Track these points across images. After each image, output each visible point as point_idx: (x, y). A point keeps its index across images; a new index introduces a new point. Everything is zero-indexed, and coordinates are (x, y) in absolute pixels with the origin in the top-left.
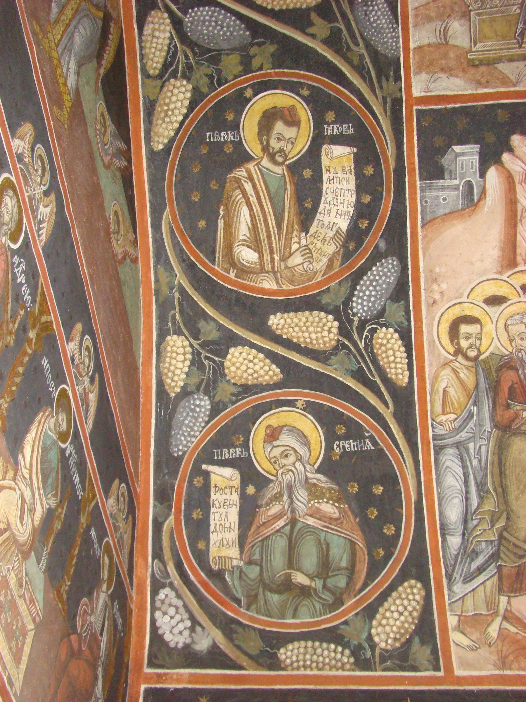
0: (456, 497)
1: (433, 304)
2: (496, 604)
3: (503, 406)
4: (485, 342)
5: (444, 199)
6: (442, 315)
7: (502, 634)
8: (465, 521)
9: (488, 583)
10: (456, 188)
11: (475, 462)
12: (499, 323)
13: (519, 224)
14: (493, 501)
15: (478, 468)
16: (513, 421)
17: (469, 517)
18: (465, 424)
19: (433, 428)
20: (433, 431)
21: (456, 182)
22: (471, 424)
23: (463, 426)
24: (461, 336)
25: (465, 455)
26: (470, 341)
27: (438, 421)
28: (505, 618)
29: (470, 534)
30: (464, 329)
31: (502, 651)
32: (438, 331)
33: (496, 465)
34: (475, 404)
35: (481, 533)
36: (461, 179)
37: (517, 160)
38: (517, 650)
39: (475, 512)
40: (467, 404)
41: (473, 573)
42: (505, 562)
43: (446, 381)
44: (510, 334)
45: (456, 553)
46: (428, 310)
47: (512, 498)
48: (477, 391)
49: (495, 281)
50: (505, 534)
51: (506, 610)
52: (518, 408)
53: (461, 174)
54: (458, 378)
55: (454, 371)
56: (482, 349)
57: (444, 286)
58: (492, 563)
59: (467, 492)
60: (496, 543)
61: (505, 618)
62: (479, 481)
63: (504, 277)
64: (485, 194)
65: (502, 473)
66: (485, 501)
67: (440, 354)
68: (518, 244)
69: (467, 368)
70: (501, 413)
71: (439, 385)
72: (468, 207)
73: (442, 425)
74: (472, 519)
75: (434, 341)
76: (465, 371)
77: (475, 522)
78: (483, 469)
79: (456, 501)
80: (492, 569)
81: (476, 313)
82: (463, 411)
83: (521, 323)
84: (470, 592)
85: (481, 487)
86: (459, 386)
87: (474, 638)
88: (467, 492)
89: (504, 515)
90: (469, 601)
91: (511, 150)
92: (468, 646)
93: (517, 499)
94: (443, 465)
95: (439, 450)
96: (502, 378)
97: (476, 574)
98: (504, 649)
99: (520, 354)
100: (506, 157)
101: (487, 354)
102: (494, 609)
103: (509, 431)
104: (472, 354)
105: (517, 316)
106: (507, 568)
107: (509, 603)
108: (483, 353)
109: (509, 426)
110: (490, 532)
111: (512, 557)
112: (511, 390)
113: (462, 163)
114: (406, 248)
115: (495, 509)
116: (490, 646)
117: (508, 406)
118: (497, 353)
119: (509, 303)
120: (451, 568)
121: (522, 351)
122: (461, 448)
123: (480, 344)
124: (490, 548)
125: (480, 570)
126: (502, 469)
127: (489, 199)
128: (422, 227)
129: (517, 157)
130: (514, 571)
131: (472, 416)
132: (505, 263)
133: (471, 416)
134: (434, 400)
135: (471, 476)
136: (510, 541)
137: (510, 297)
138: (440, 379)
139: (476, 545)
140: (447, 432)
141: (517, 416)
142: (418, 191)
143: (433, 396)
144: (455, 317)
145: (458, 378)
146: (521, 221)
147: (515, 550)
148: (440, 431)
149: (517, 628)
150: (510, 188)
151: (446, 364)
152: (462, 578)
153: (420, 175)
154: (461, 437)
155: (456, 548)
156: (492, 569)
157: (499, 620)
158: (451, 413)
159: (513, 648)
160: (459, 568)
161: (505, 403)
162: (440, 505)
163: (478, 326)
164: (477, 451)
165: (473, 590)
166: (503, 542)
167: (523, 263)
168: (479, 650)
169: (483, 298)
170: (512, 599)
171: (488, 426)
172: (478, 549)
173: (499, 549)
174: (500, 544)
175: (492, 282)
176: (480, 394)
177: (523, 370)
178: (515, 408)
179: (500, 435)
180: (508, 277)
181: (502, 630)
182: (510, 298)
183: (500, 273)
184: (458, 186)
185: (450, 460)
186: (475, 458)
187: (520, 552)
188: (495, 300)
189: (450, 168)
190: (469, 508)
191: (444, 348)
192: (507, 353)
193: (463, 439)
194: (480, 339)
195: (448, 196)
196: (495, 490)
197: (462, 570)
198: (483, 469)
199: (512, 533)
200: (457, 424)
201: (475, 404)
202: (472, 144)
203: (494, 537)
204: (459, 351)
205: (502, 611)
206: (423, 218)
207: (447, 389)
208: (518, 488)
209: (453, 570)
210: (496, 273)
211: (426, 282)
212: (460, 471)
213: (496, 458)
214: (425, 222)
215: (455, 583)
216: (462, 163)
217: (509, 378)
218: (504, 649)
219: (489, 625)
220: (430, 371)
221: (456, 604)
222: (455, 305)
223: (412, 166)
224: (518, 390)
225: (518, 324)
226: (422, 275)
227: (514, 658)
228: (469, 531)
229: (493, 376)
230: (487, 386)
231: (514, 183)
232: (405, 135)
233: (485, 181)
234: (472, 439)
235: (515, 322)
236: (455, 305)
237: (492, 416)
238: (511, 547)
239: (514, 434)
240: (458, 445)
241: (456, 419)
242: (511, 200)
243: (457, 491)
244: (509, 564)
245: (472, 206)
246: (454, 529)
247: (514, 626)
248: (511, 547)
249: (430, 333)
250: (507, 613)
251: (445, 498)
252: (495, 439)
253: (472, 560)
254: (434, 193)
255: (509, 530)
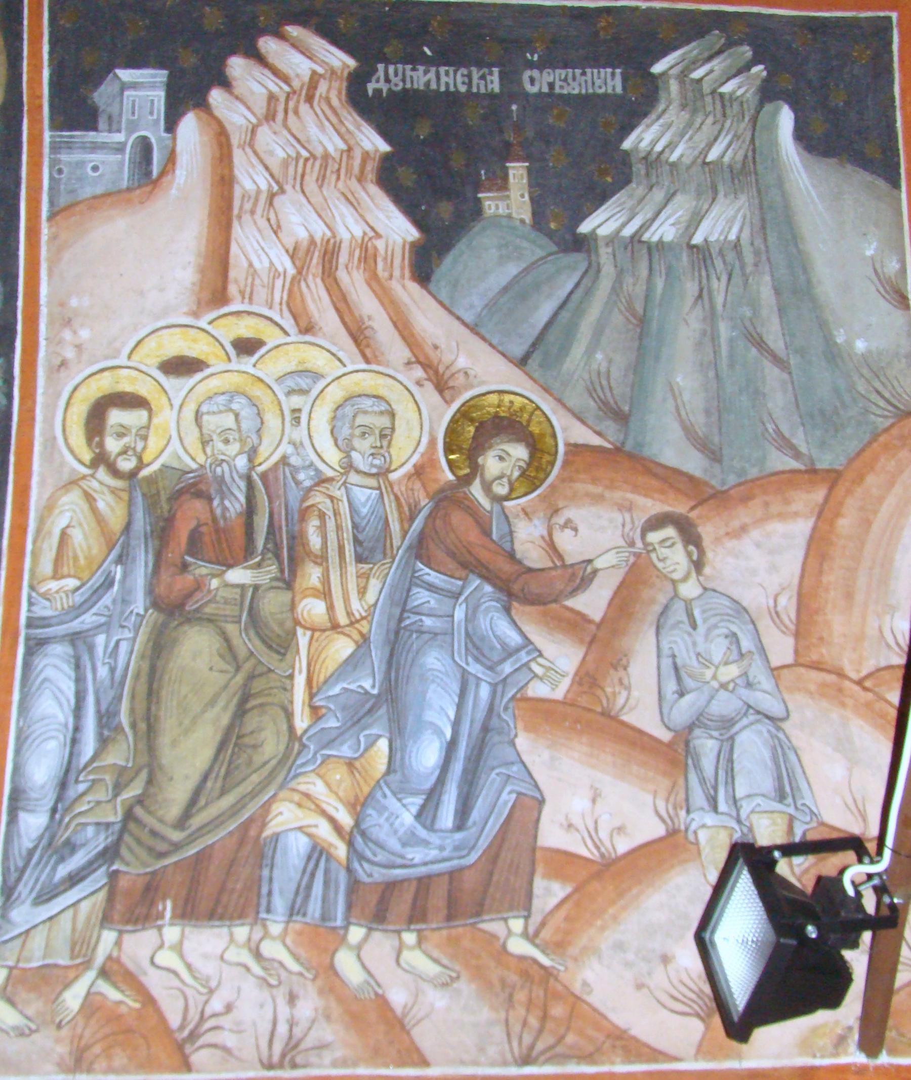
0: (52, 738)
1: (60, 366)
2: (92, 945)
3: (176, 565)
4: (154, 443)
5: (95, 169)
6: (75, 389)
7: (92, 1005)
8: (63, 785)
9: (85, 906)
10: (120, 148)
11: (103, 672)
12: (185, 409)
13: (235, 224)
14: (125, 746)
15: (107, 683)
16: (189, 595)
17: (72, 776)
18: (94, 598)
19: (31, 603)
20: (29, 611)
21: (119, 137)
22: (107, 600)
23: (90, 603)
24: (108, 430)
25: (86, 658)
26: (126, 440)
27: (43, 590)
28: (104, 973)
29: (67, 810)
30: (116, 417)
31: (81, 1037)
32: (64, 420)
33: (144, 679)
34: (120, 560)
35: (92, 809)
36: (130, 132)
37: (238, 104)
38: (113, 1034)
39: (85, 767)
40: (104, 561)
41: (56, 886)
42: (128, 864)
43: (68, 514)
44: (205, 431)
45: (31, 845)
46: (49, 378)
47: (164, 741)
48: (128, 537)
49: (184, 329)
50: (139, 811)
51: (109, 958)
52: (204, 571)
53: (130, 122)
54: (94, 510)
55: (89, 498)
56: (146, 459)
57: (85, 334)
58: (100, 866)
59: (77, 729)
60: (117, 827)
61: (104, 973)
62: (104, 707)
63: (203, 323)
64: (174, 164)
65: (152, 694)
66: (110, 747)
67: (63, 464)
68: (232, 261)
69: (113, 491)
70: (169, 580)
71: (53, 522)
72: (139, 187)
73: (48, 599)
74: (77, 781)
75: (55, 438)
76: (109, 498)
77: (82, 787)
78: (116, 685)
79: (52, 745)
80: (99, 878)
81: (144, 388)
82: (93, 575)
83: (226, 411)
84: (44, 922)
85: (107, 719)
86: (94, 524)
87: (30, 1012)
88: (77, 729)
89: (144, 775)
90: (37, 941)
91: (225, 83)
92: (15, 1028)
93: (174, 743)
94: (38, 676)
95: (36, 646)
96: (179, 514)
97: (62, 888)
98: (87, 1033)
99: (219, 470)
100: (216, 96)
101: (155, 467)
102: (85, 956)
103: (180, 615)
104: (126, 465)
105: (223, 397)
106: (128, 877)
107: (118, 943)
108: (148, 465)
109: (182, 605)
110: (109, 807)
111: (143, 854)
112: (195, 539)
113: (134, 102)
114: (16, 256)
115: (127, 760)
116: (59, 1026)
117: (185, 567)
118: (175, 464)
119: (208, 372)
120: (14, 876)
121: (225, 465)
122: (80, 644)
123: (144, 448)
124: (102, 837)
125: (74, 880)
126: (155, 686)
127: (181, 173)
128: (50, 219)
129: (237, 98)
130: (140, 883)
131: (112, 584)
132: (206, 295)
133: (109, 582)
134: (41, 548)
135: (91, 699)
136: (145, 826)
137: (211, 360)
138: (56, 511)
139: (75, 832)
140: (57, 613)
141: (199, 585)
142: (46, 150)
143: (38, 544)
144: (100, 395)
145: (94, 510)
146: (239, 217)
147: (151, 841)
148: (43, 610)
149: (122, 992)
150: (222, 155)
151: (74, 482)
152: (34, 895)
153: (52, 119)
154: (83, 622)
155: (35, 834)
156: (99, 878)
157: (91, 975)
158: (69, 576)
159: (107, 1030)
160: (32, 873)
161: (178, 561)
162: (18, 752)
163: (144, 413)
164: (110, 650)
165: (51, 918)
166: (132, 826)
167: (239, 298)
168: (35, 1036)
169: (159, 360)
170: (126, 937)
171: (139, 604)
172: (79, 839)
173: (120, 839)
174: (124, 829)
175: (178, 330)
176: (133, 542)
177: (222, 499)
178: (197, 572)
179: (160, 621)
180: (210, 323)
181: (91, 997)
182: (210, 363)
183: (196, 314)
184: (124, 144)
185: (55, 667)
186: (104, 664)
187: (162, 847)
188: (181, 366)
189: (109, 109)
190: (74, 761)
191: (72, 452)
192: (194, 466)
193: (86, 627)
194: (145, 438)
195: (103, 162)
196: (133, 726)
197: (37, 880)
198: (116, 685)
199: (152, 808)
200: (78, 598)
201: (120, 560)
202: (154, 68)
203: (115, 817)
204: (101, 459)
205: (100, 958)
206: (52, 203)
207: (69, 531)
208: (180, 724)
209: (19, 879)
210: (187, 314)
211: (51, 323)
212: (69, 688)
213: (146, 666)
214: (56, 209)
215: (18, 902)
216: (134, 102)
217: (193, 511)
218: (87, 1033)
219: (67, 985)
220: (40, 494)
221: (9, 945)
222: (102, 370)
223: (37, 102)
224: (207, 539)
225: (221, 412)
226: (44, 311)
227: (104, 1051)
228: (67, 803)
229: (161, 508)
230: (148, 528)
231: (229, 146)
232: (26, 43)
233: (174, 139)
234: (105, 628)
235: (215, 409)
236: (102, 370)
237: (151, 584)
238: (145, 837)
239: (188, 621)
240: (78, 640)
241: (78, 589)
242: (222, 178)
243: (57, 726)
244: (133, 868)
245: (147, 185)
246: (37, 800)
247: (117, 988)
248: (145, 837)
249: (49, 421)
250: (109, 964)
251: (29, 741)
252: (149, 629)
253: (62, 859)
254: (76, 156)
255: (147, 803)
